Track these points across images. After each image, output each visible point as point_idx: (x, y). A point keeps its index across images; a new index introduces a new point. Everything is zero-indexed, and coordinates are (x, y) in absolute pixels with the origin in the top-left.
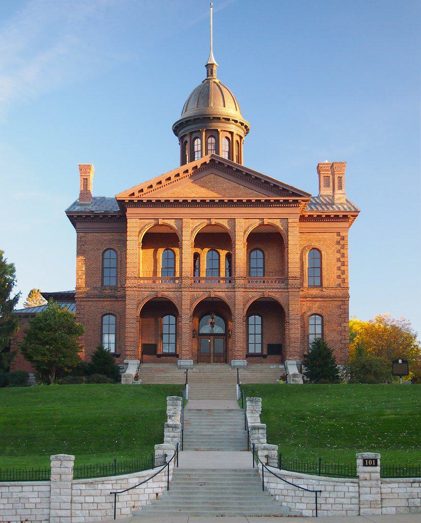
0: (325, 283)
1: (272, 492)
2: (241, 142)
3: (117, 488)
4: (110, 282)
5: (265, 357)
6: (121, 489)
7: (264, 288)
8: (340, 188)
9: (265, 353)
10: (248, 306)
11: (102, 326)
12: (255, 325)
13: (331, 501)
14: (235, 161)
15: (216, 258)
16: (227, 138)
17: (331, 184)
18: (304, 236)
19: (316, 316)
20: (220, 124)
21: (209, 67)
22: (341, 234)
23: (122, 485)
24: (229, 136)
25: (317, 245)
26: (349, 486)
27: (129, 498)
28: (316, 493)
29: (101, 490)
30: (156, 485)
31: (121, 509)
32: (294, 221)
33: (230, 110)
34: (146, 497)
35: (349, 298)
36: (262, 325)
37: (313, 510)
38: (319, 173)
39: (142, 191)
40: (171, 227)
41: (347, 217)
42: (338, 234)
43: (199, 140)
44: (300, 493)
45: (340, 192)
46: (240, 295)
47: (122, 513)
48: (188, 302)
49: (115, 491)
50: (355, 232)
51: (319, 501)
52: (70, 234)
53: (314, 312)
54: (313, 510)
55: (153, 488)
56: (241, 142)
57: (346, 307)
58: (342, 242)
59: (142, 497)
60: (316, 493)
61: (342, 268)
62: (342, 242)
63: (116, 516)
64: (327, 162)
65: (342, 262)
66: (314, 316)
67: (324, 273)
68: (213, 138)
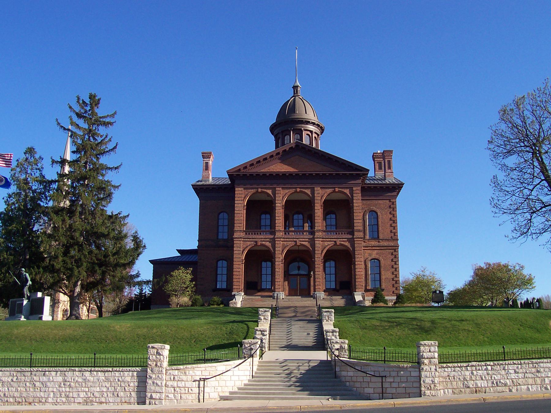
0: (381, 236)
1: (343, 379)
2: (318, 138)
3: (206, 374)
4: (223, 235)
5: (338, 291)
6: (210, 375)
7: (336, 238)
8: (390, 168)
9: (338, 288)
10: (325, 251)
11: (217, 269)
12: (330, 267)
13: (394, 385)
14: (314, 146)
15: (301, 225)
16: (307, 134)
17: (383, 168)
18: (364, 202)
19: (375, 260)
20: (303, 125)
21: (295, 88)
22: (391, 200)
23: (211, 372)
24: (310, 134)
25: (375, 209)
26: (410, 371)
27: (216, 384)
28: (382, 378)
29: (192, 376)
30: (241, 373)
31: (209, 393)
32: (357, 190)
33: (311, 116)
34: (232, 383)
35: (398, 246)
36: (335, 267)
37: (379, 394)
38: (374, 160)
39: (246, 167)
40: (268, 195)
41: (397, 187)
42: (390, 201)
43: (288, 136)
44: (367, 379)
45: (390, 171)
46: (319, 244)
47: (211, 397)
48: (281, 249)
49: (204, 377)
50: (401, 200)
51: (385, 385)
52: (195, 201)
53: (374, 257)
54: (379, 394)
55: (239, 376)
56: (318, 138)
57: (396, 253)
58: (392, 206)
59: (228, 383)
60: (382, 378)
61: (393, 225)
62: (393, 208)
63: (205, 400)
64: (379, 152)
65: (393, 221)
66: (373, 260)
67: (380, 229)
68: (298, 135)
